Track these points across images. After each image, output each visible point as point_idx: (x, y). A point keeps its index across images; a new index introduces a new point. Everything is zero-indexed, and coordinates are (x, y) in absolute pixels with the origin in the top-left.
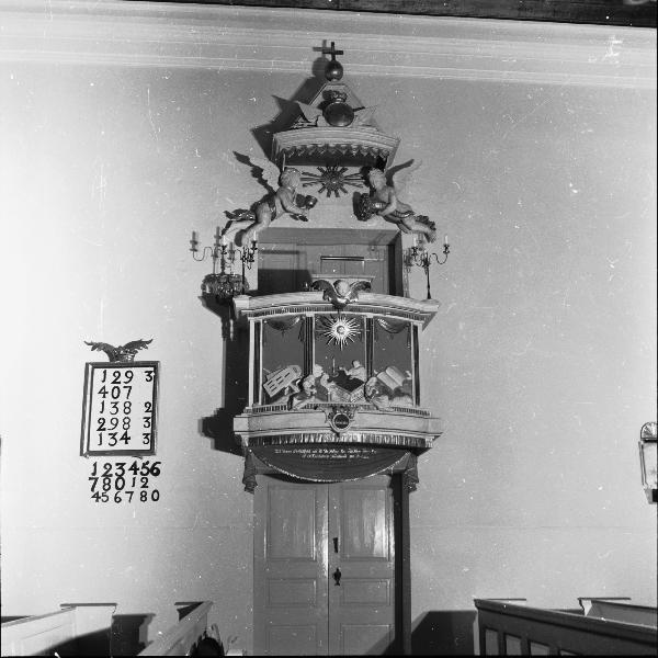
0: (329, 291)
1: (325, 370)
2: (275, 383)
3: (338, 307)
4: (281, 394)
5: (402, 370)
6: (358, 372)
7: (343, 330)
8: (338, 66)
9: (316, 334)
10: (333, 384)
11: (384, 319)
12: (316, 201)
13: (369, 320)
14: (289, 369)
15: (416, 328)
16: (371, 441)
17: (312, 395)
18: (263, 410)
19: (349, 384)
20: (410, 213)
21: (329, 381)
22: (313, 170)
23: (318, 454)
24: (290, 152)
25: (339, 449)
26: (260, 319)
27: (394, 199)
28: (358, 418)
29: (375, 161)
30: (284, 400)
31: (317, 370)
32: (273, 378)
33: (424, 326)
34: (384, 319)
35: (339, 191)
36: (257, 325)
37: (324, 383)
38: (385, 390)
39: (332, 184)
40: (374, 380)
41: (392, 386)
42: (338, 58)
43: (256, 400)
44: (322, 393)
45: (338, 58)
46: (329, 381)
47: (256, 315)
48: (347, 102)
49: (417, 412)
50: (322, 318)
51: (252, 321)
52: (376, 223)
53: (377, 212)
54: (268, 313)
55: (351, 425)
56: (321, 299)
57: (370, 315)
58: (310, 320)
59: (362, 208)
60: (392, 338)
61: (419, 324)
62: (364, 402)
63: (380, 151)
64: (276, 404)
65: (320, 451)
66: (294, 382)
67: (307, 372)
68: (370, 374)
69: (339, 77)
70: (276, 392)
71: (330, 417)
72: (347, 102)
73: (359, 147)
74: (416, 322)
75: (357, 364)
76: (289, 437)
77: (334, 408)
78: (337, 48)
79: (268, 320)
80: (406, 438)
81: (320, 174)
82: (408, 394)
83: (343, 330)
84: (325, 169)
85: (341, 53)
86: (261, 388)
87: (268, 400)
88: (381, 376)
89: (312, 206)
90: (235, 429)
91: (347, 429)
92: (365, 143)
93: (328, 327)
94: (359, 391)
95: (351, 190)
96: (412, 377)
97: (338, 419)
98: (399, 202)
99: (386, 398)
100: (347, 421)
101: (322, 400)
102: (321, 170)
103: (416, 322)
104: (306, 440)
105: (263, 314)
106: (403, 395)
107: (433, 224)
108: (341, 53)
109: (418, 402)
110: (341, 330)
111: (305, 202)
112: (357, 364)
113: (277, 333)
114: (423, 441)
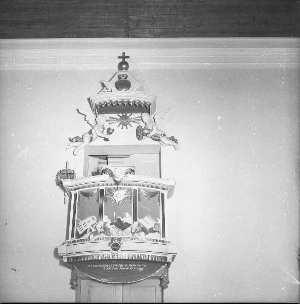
0: (111, 175)
1: (109, 218)
2: (83, 226)
3: (117, 183)
4: (85, 232)
5: (155, 217)
6: (128, 218)
7: (119, 195)
8: (126, 63)
9: (106, 198)
10: (113, 226)
11: (144, 189)
12: (113, 130)
13: (135, 191)
14: (90, 218)
15: (163, 195)
16: (134, 258)
17: (101, 233)
18: (75, 241)
19: (122, 226)
20: (164, 135)
21: (111, 224)
22: (115, 116)
23: (112, 267)
24: (99, 105)
25: (136, 264)
26: (77, 191)
27: (155, 128)
28: (125, 245)
29: (145, 108)
30: (86, 237)
31: (105, 218)
32: (81, 223)
33: (169, 196)
34: (144, 189)
35: (128, 125)
36: (76, 195)
37: (108, 225)
38: (144, 230)
39: (125, 122)
40: (136, 223)
41: (148, 227)
42: (126, 60)
43: (72, 236)
44: (106, 230)
45: (126, 60)
46: (111, 224)
47: (75, 190)
48: (128, 79)
49: (163, 241)
50: (109, 190)
51: (73, 193)
52: (147, 141)
53: (146, 134)
54: (80, 188)
55: (122, 248)
56: (108, 179)
57: (136, 188)
58: (102, 190)
59: (140, 133)
60: (149, 199)
61: (166, 193)
62: (130, 235)
63: (145, 103)
64: (82, 238)
65: (114, 266)
66: (92, 226)
67: (100, 218)
68: (135, 219)
69: (127, 69)
70: (82, 232)
71: (110, 244)
72: (128, 79)
73: (134, 101)
74: (162, 191)
75: (127, 214)
76: (81, 257)
77: (112, 239)
78: (126, 55)
79: (81, 192)
80: (156, 257)
81: (119, 118)
82: (158, 232)
83: (119, 195)
84: (121, 115)
85: (128, 57)
86: (75, 229)
87: (79, 236)
88: (141, 221)
89: (111, 133)
90: (58, 253)
91: (119, 251)
92: (137, 99)
93: (112, 194)
94: (129, 229)
95: (135, 126)
96: (160, 222)
97: (114, 245)
98: (157, 129)
99: (143, 233)
100: (119, 246)
101: (107, 235)
102: (119, 116)
103: (162, 191)
104: (83, 260)
105: (78, 189)
106: (155, 231)
107: (177, 140)
108: (128, 57)
109: (164, 236)
110: (119, 196)
111: (110, 131)
112: (127, 214)
113: (86, 199)
114: (166, 258)
